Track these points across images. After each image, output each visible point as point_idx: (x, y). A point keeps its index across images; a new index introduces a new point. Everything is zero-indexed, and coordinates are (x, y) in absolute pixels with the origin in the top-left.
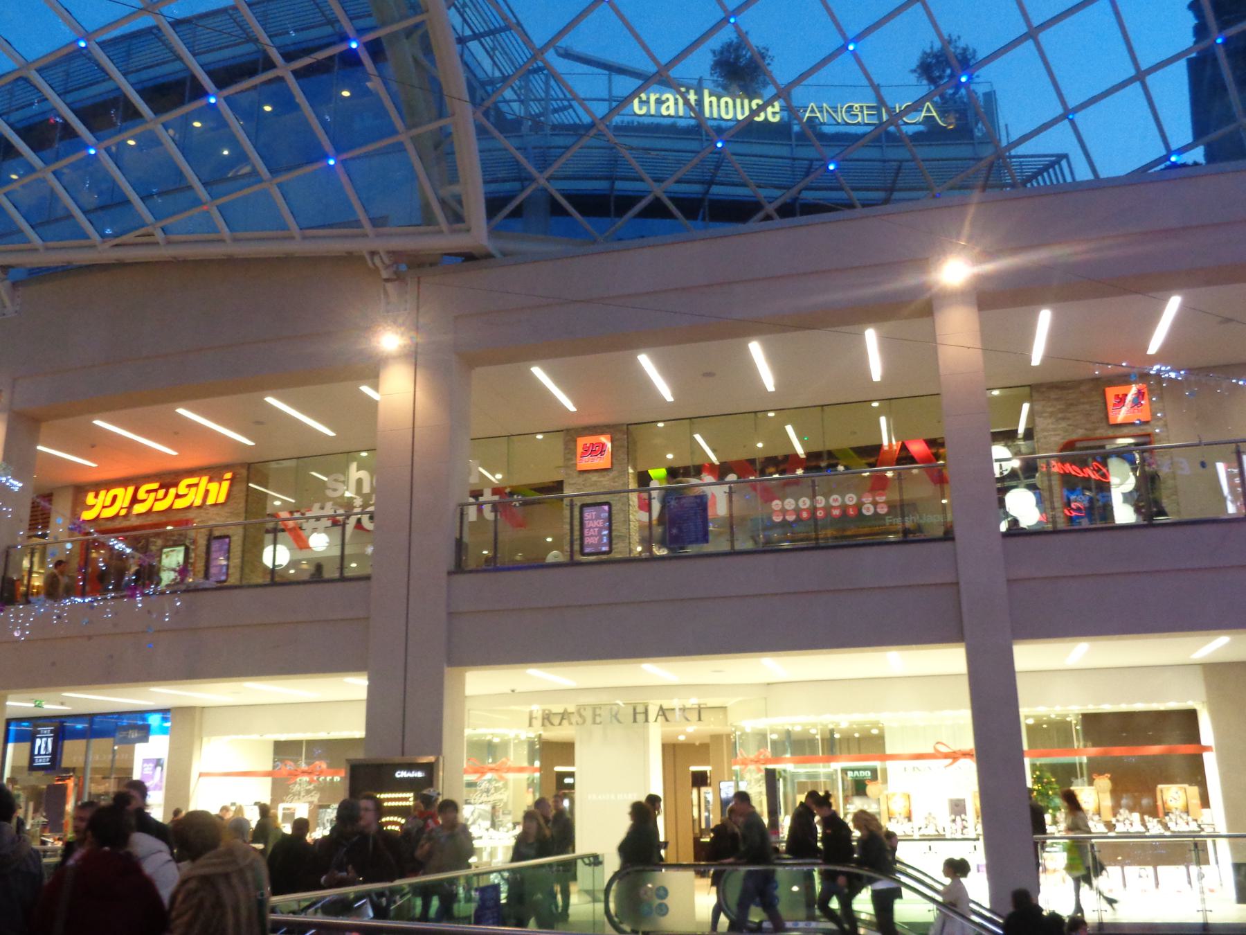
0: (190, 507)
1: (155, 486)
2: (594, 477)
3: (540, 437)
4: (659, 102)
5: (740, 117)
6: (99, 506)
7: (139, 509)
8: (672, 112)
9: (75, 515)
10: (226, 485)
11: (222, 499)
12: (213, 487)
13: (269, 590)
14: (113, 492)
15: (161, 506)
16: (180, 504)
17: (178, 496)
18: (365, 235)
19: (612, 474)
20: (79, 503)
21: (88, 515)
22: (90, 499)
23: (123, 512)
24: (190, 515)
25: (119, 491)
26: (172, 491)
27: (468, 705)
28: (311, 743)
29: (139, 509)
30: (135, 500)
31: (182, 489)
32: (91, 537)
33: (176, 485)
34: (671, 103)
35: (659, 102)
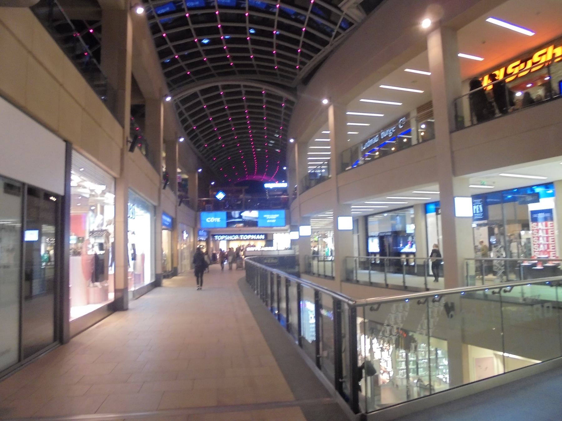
1: (518, 63)
33: (531, 58)
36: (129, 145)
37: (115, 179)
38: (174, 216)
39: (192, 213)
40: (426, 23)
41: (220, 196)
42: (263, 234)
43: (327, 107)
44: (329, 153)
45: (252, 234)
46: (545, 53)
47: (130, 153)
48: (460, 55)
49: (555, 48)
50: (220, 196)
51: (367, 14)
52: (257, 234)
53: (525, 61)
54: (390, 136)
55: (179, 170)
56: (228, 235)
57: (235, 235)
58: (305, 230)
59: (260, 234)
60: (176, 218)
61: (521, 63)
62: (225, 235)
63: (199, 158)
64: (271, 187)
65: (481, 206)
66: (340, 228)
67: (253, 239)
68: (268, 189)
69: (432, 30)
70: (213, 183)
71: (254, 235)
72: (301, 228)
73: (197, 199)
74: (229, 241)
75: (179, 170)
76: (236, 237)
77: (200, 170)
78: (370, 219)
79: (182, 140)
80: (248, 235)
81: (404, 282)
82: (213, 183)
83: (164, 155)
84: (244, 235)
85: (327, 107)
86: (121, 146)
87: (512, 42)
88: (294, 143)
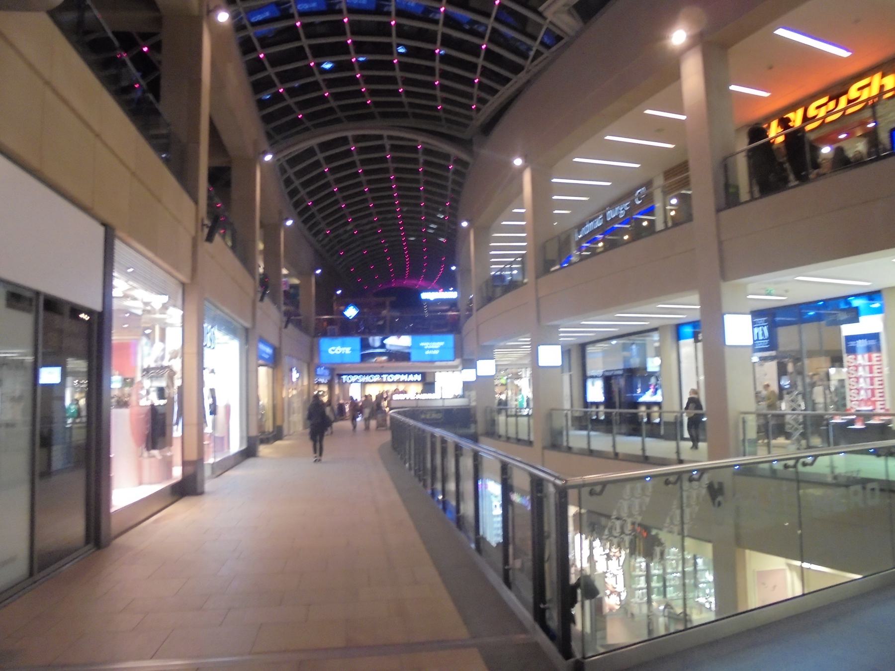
1: (824, 100)
33: (846, 92)
36: (206, 231)
37: (183, 285)
38: (276, 344)
39: (306, 339)
40: (678, 37)
41: (351, 312)
42: (418, 374)
43: (521, 171)
44: (525, 244)
45: (401, 374)
46: (869, 85)
47: (207, 244)
48: (733, 88)
49: (883, 76)
50: (351, 312)
51: (585, 22)
52: (409, 374)
53: (836, 97)
54: (621, 216)
55: (285, 271)
56: (363, 374)
57: (375, 374)
58: (486, 367)
59: (414, 374)
60: (280, 348)
61: (830, 100)
62: (358, 375)
63: (316, 251)
64: (432, 299)
65: (765, 329)
66: (542, 363)
67: (404, 382)
68: (427, 301)
69: (688, 48)
70: (339, 292)
71: (405, 374)
72: (480, 363)
73: (313, 317)
74: (364, 384)
75: (285, 271)
76: (376, 378)
77: (318, 272)
78: (590, 349)
79: (289, 223)
80: (394, 374)
81: (643, 450)
82: (339, 292)
83: (261, 246)
84: (389, 374)
85: (521, 171)
86: (193, 233)
87: (815, 67)
88: (468, 228)
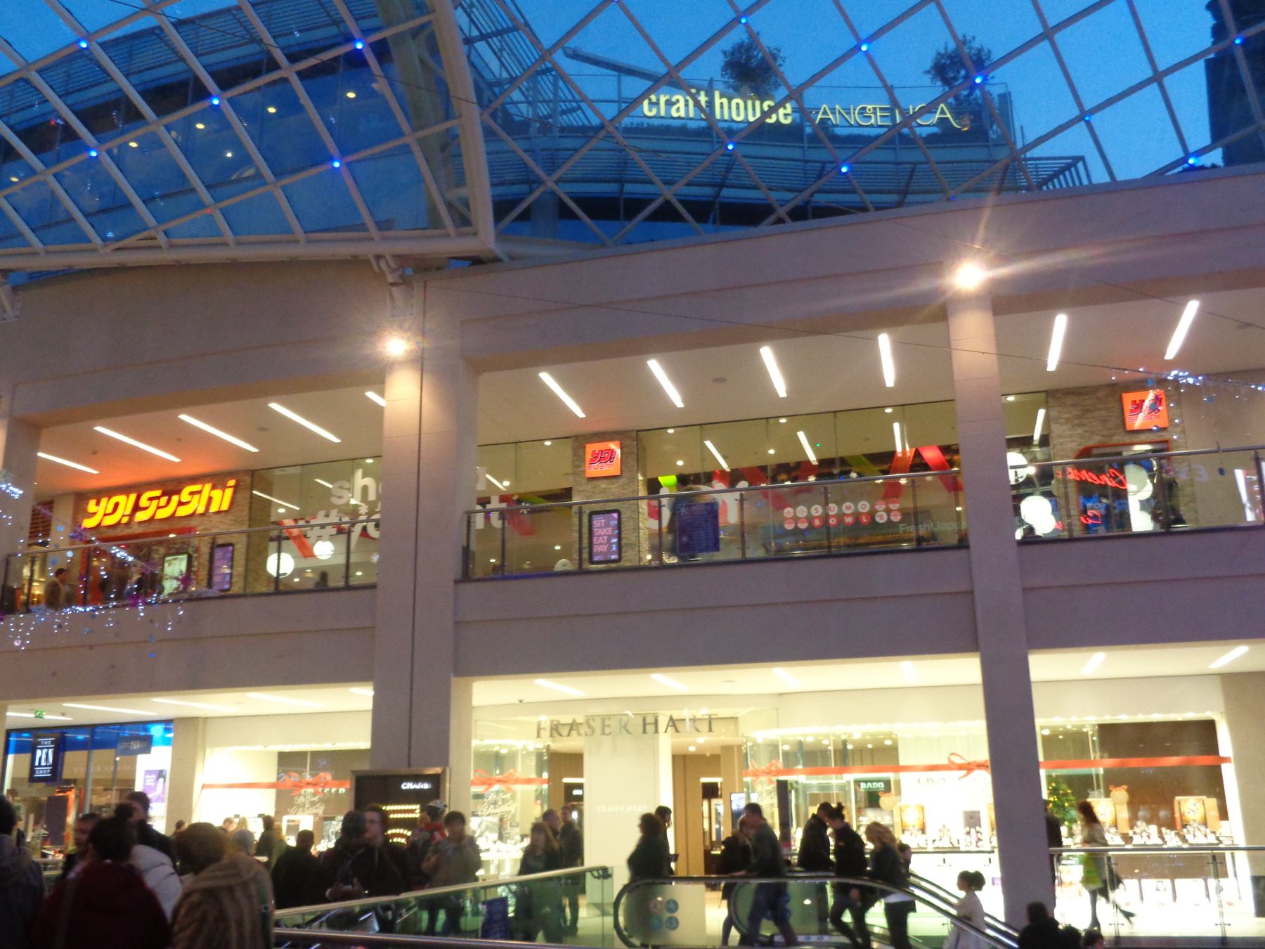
0: (193, 515)
1: (157, 493)
2: (603, 484)
3: (548, 443)
4: (669, 104)
5: (751, 119)
6: (100, 514)
7: (141, 516)
8: (682, 114)
9: (76, 522)
10: (229, 492)
11: (225, 507)
12: (217, 494)
13: (273, 598)
14: (114, 499)
15: (163, 514)
16: (183, 511)
17: (180, 504)
18: (371, 239)
19: (621, 482)
20: (80, 511)
21: (89, 523)
22: (92, 506)
23: (125, 520)
24: (193, 523)
25: (121, 499)
26: (175, 499)
27: (475, 715)
28: (316, 754)
29: (141, 516)
30: (137, 508)
31: (185, 496)
32: (92, 545)
33: (178, 492)
34: (681, 104)
35: (669, 104)
